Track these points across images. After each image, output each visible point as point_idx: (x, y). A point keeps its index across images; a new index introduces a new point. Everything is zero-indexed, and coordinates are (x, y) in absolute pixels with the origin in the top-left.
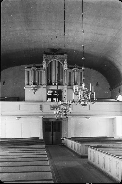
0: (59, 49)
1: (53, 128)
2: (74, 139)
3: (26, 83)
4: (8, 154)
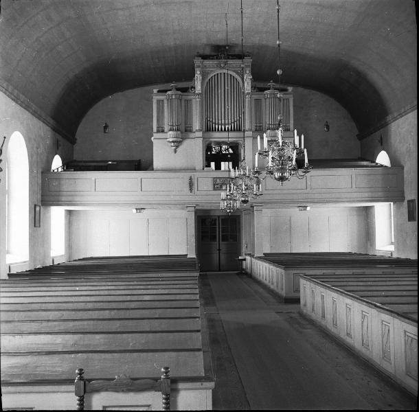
0: (232, 46)
1: (218, 232)
2: (268, 258)
3: (155, 129)
4: (113, 292)
